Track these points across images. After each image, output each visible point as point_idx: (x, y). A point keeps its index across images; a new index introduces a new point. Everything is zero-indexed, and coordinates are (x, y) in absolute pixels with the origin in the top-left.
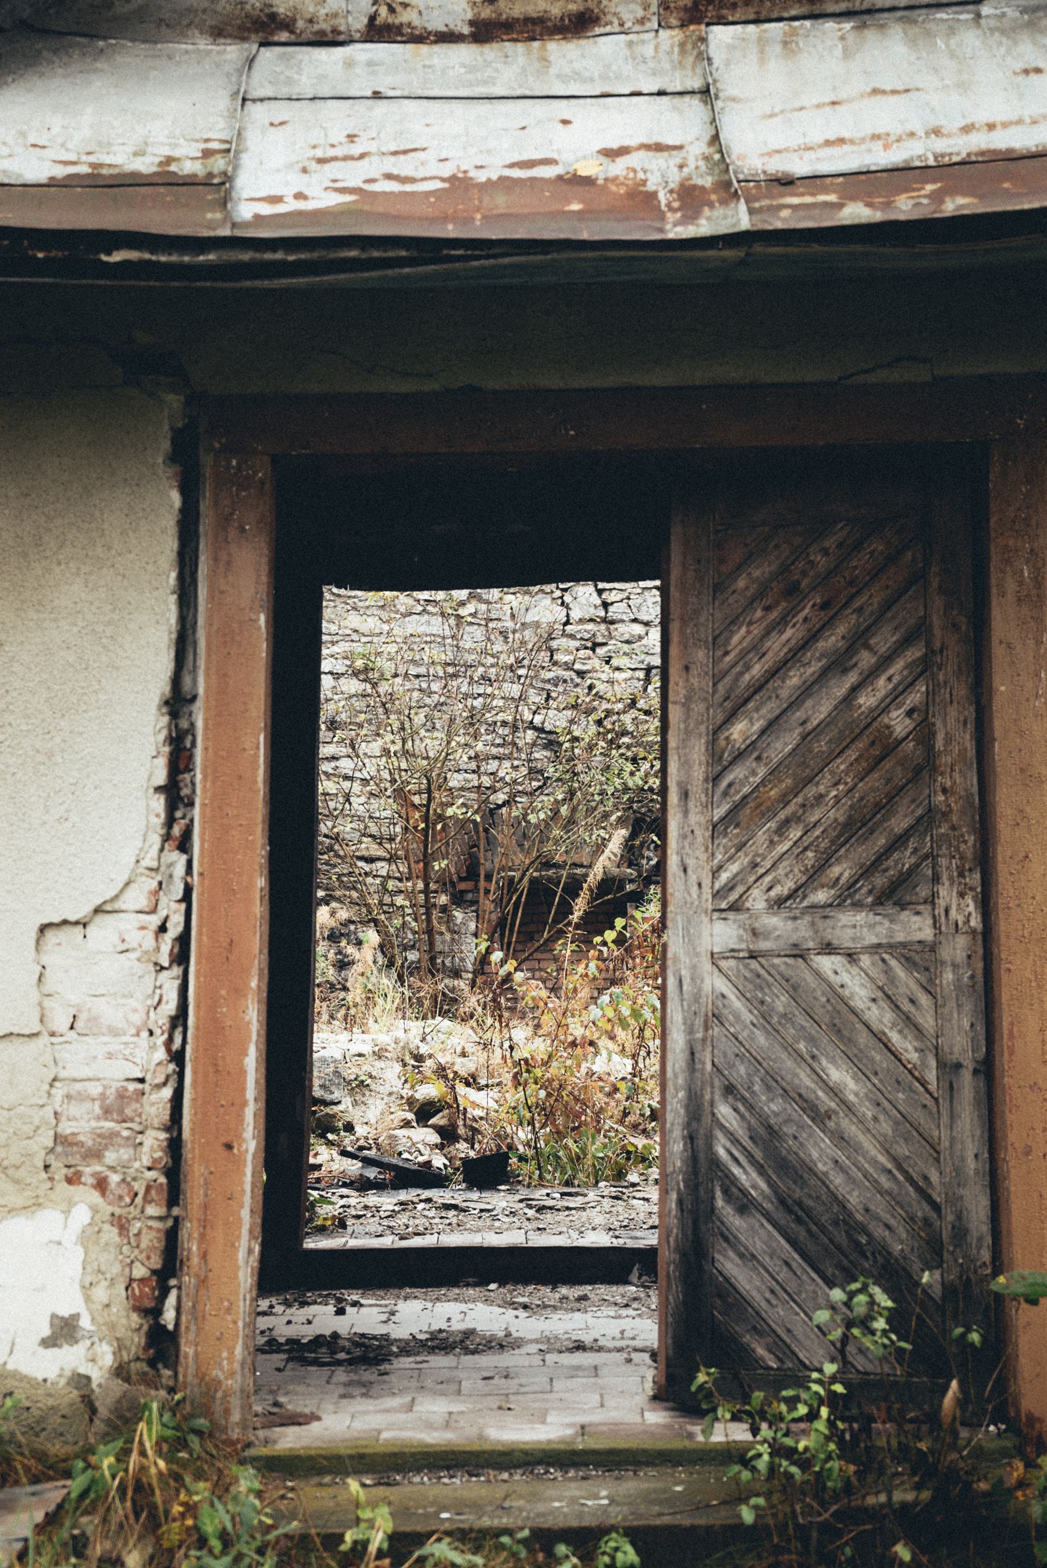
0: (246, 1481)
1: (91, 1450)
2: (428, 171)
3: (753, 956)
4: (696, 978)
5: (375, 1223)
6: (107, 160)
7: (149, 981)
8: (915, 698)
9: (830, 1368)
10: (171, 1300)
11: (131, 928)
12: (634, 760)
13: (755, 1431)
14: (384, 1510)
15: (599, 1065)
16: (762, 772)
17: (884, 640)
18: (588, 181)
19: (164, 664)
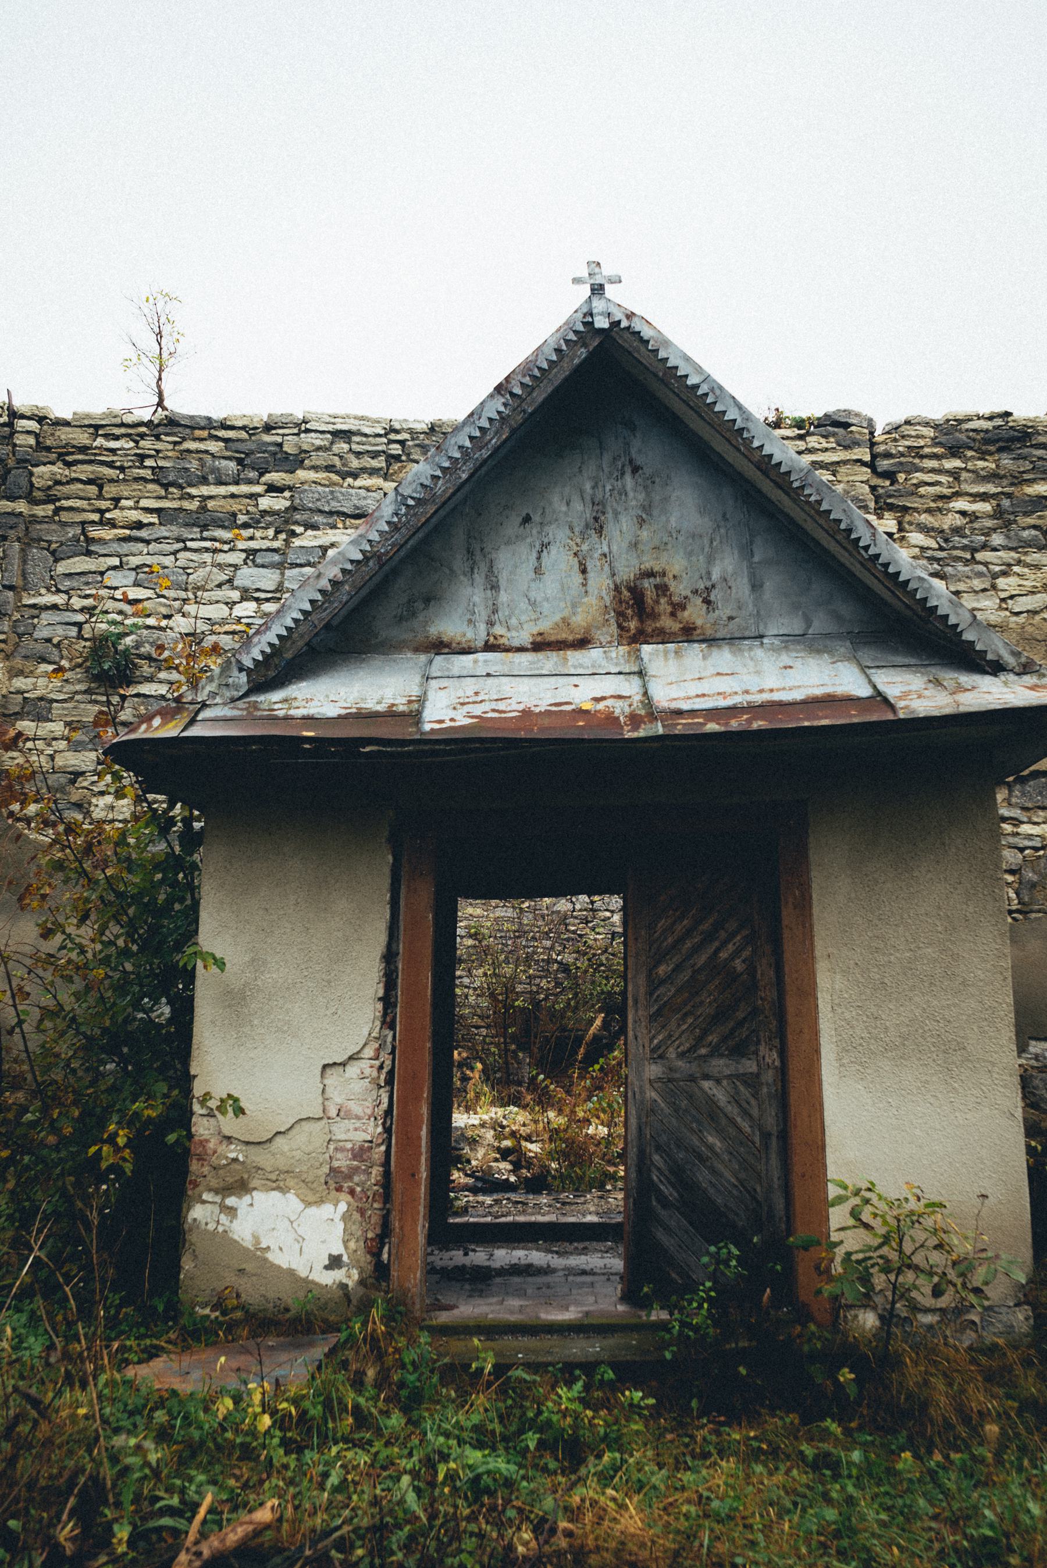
0: (424, 1338)
1: (350, 1320)
2: (512, 707)
3: (670, 1080)
4: (642, 1092)
5: (480, 1209)
6: (363, 706)
7: (374, 1093)
8: (746, 954)
9: (708, 1284)
10: (386, 1249)
11: (365, 1066)
12: (607, 978)
13: (671, 1314)
14: (491, 1353)
15: (591, 1131)
16: (673, 990)
17: (732, 925)
18: (587, 712)
19: (383, 938)
